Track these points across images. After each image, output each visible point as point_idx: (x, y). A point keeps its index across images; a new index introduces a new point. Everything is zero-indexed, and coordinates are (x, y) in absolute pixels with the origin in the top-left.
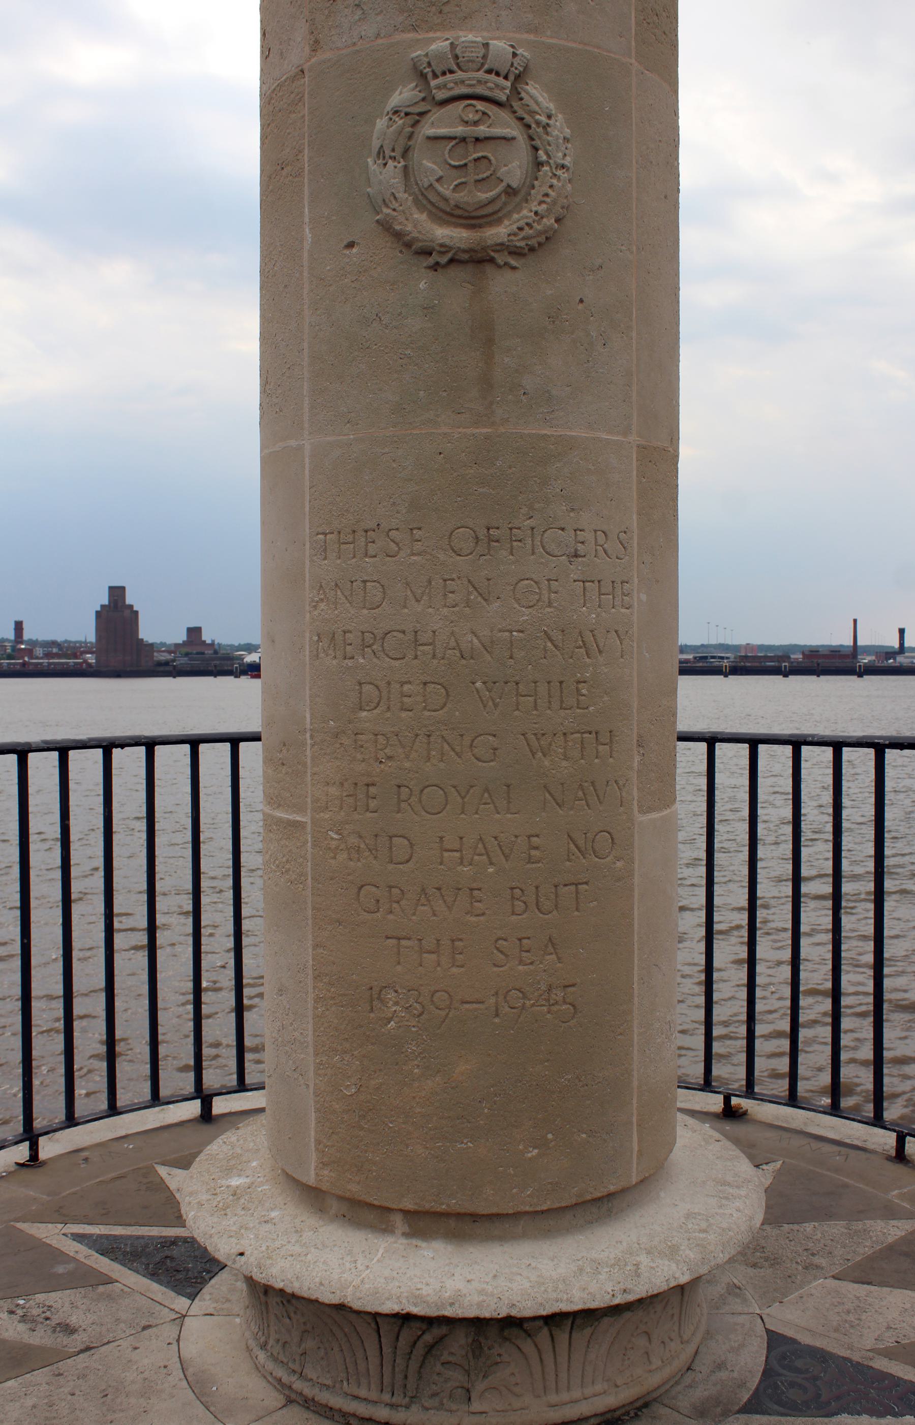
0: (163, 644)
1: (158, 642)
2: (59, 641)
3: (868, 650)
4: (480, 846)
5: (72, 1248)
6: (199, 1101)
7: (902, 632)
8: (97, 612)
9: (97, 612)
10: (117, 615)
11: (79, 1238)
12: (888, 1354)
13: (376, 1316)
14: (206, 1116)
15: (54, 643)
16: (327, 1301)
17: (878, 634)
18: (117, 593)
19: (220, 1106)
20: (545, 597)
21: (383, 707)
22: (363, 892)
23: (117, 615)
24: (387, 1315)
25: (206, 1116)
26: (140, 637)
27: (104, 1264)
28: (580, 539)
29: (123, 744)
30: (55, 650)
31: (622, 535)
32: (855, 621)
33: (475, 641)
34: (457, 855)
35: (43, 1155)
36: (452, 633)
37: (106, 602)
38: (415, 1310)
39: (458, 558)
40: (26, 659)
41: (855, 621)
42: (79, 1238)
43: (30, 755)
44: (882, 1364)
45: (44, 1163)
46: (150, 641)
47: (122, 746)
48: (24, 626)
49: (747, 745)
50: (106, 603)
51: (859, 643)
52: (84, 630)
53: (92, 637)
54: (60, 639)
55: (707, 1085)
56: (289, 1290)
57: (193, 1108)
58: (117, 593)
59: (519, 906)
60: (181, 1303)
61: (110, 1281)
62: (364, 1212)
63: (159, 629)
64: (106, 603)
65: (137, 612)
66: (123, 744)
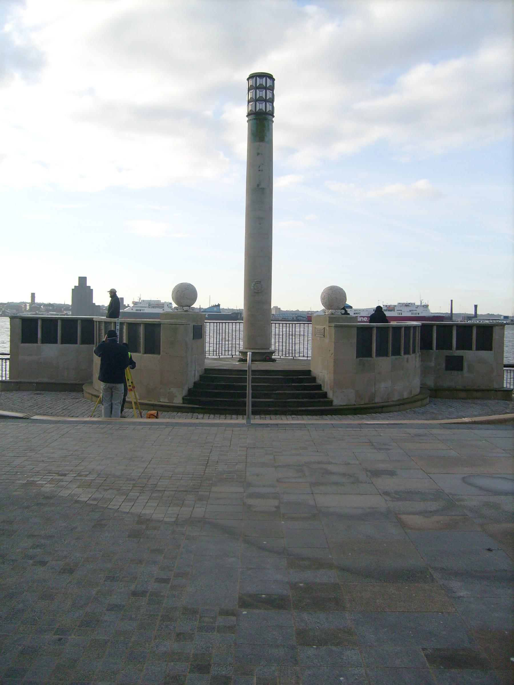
2: (52, 303)
7: (476, 306)
18: (83, 280)
30: (51, 308)
32: (452, 301)
41: (452, 301)
48: (36, 296)
50: (77, 285)
51: (453, 312)
53: (69, 302)
58: (83, 280)
64: (77, 285)
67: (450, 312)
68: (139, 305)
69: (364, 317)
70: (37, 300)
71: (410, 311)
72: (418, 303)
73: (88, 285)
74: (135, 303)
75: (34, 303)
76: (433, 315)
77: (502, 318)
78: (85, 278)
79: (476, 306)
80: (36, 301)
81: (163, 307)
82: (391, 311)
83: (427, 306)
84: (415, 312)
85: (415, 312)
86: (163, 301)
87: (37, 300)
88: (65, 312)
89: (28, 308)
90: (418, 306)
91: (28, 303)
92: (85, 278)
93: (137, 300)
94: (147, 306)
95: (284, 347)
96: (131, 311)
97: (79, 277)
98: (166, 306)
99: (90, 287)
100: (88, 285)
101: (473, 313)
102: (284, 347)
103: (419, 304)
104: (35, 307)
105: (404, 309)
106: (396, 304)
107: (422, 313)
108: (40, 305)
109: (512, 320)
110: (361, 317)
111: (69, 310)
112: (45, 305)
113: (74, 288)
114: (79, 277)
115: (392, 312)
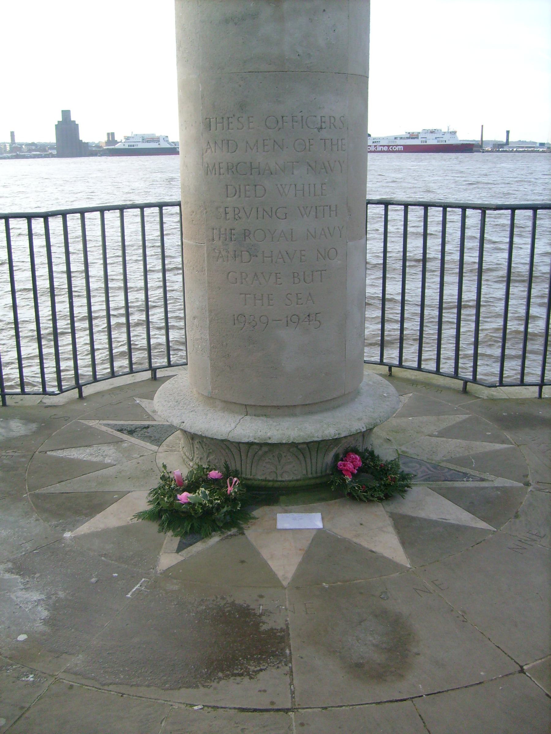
0: (93, 143)
1: (91, 142)
2: (36, 142)
3: (488, 142)
4: (280, 255)
5: (104, 428)
6: (150, 371)
7: (508, 132)
8: (56, 125)
9: (56, 125)
10: (67, 129)
11: (108, 425)
12: (447, 461)
13: (239, 443)
14: (154, 378)
15: (33, 144)
16: (219, 438)
17: (495, 135)
18: (66, 114)
19: (159, 374)
20: (307, 148)
21: (237, 196)
22: (230, 275)
23: (67, 129)
24: (244, 443)
25: (154, 378)
26: (80, 139)
27: (119, 434)
28: (323, 120)
29: (110, 208)
30: (33, 147)
31: (342, 118)
32: (482, 126)
33: (277, 167)
34: (270, 259)
35: (84, 395)
36: (267, 164)
37: (61, 120)
38: (256, 441)
39: (269, 130)
40: (18, 153)
41: (482, 126)
42: (108, 425)
43: (68, 215)
44: (443, 464)
45: (86, 397)
46: (86, 142)
47: (109, 210)
48: (15, 134)
49: (403, 206)
50: (61, 120)
51: (484, 140)
52: (49, 137)
53: (55, 142)
54: (36, 142)
55: (381, 363)
56: (203, 435)
57: (148, 375)
58: (66, 114)
59: (296, 280)
60: (155, 448)
61: (122, 441)
62: (231, 406)
63: (89, 134)
64: (61, 120)
65: (78, 125)
66: (110, 208)
67: (480, 139)
68: (131, 140)
69: (384, 146)
70: (18, 140)
71: (436, 138)
72: (445, 130)
73: (72, 119)
74: (127, 138)
75: (15, 143)
76: (462, 142)
77: (538, 145)
78: (68, 112)
79: (508, 132)
80: (16, 141)
81: (159, 141)
82: (414, 138)
83: (454, 133)
84: (441, 139)
85: (441, 139)
86: (158, 135)
87: (18, 140)
88: (50, 151)
89: (8, 148)
90: (445, 133)
91: (8, 143)
92: (68, 112)
93: (129, 135)
94: (141, 140)
95: (434, 244)
96: (122, 147)
97: (62, 111)
98: (162, 141)
99: (74, 121)
100: (72, 119)
101: (505, 141)
102: (434, 244)
103: (446, 130)
104: (16, 148)
105: (429, 136)
106: (420, 130)
107: (449, 140)
108: (21, 145)
109: (548, 148)
110: (381, 146)
111: (54, 149)
112: (27, 145)
113: (57, 123)
114: (62, 111)
115: (416, 140)
